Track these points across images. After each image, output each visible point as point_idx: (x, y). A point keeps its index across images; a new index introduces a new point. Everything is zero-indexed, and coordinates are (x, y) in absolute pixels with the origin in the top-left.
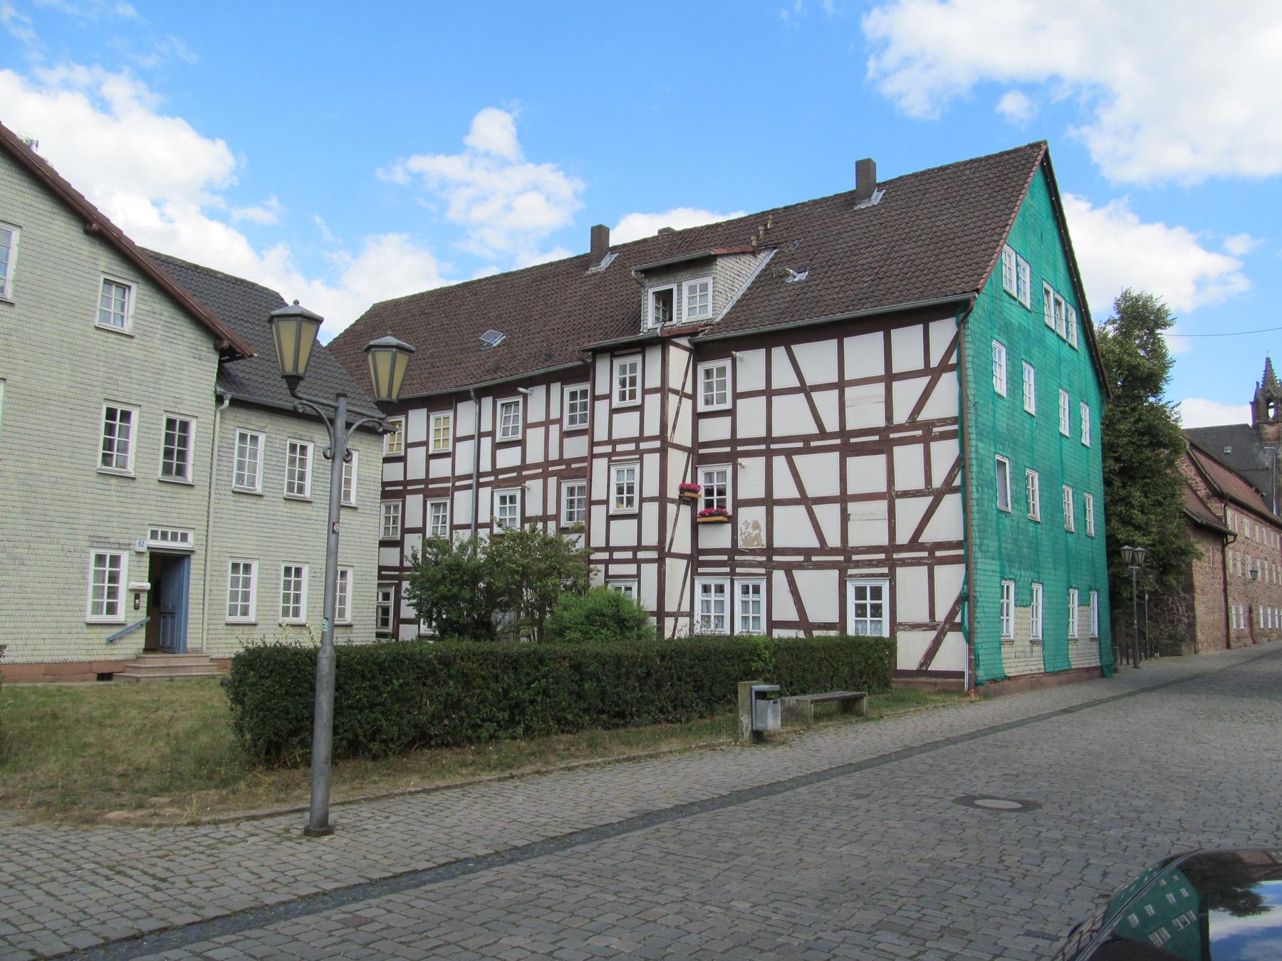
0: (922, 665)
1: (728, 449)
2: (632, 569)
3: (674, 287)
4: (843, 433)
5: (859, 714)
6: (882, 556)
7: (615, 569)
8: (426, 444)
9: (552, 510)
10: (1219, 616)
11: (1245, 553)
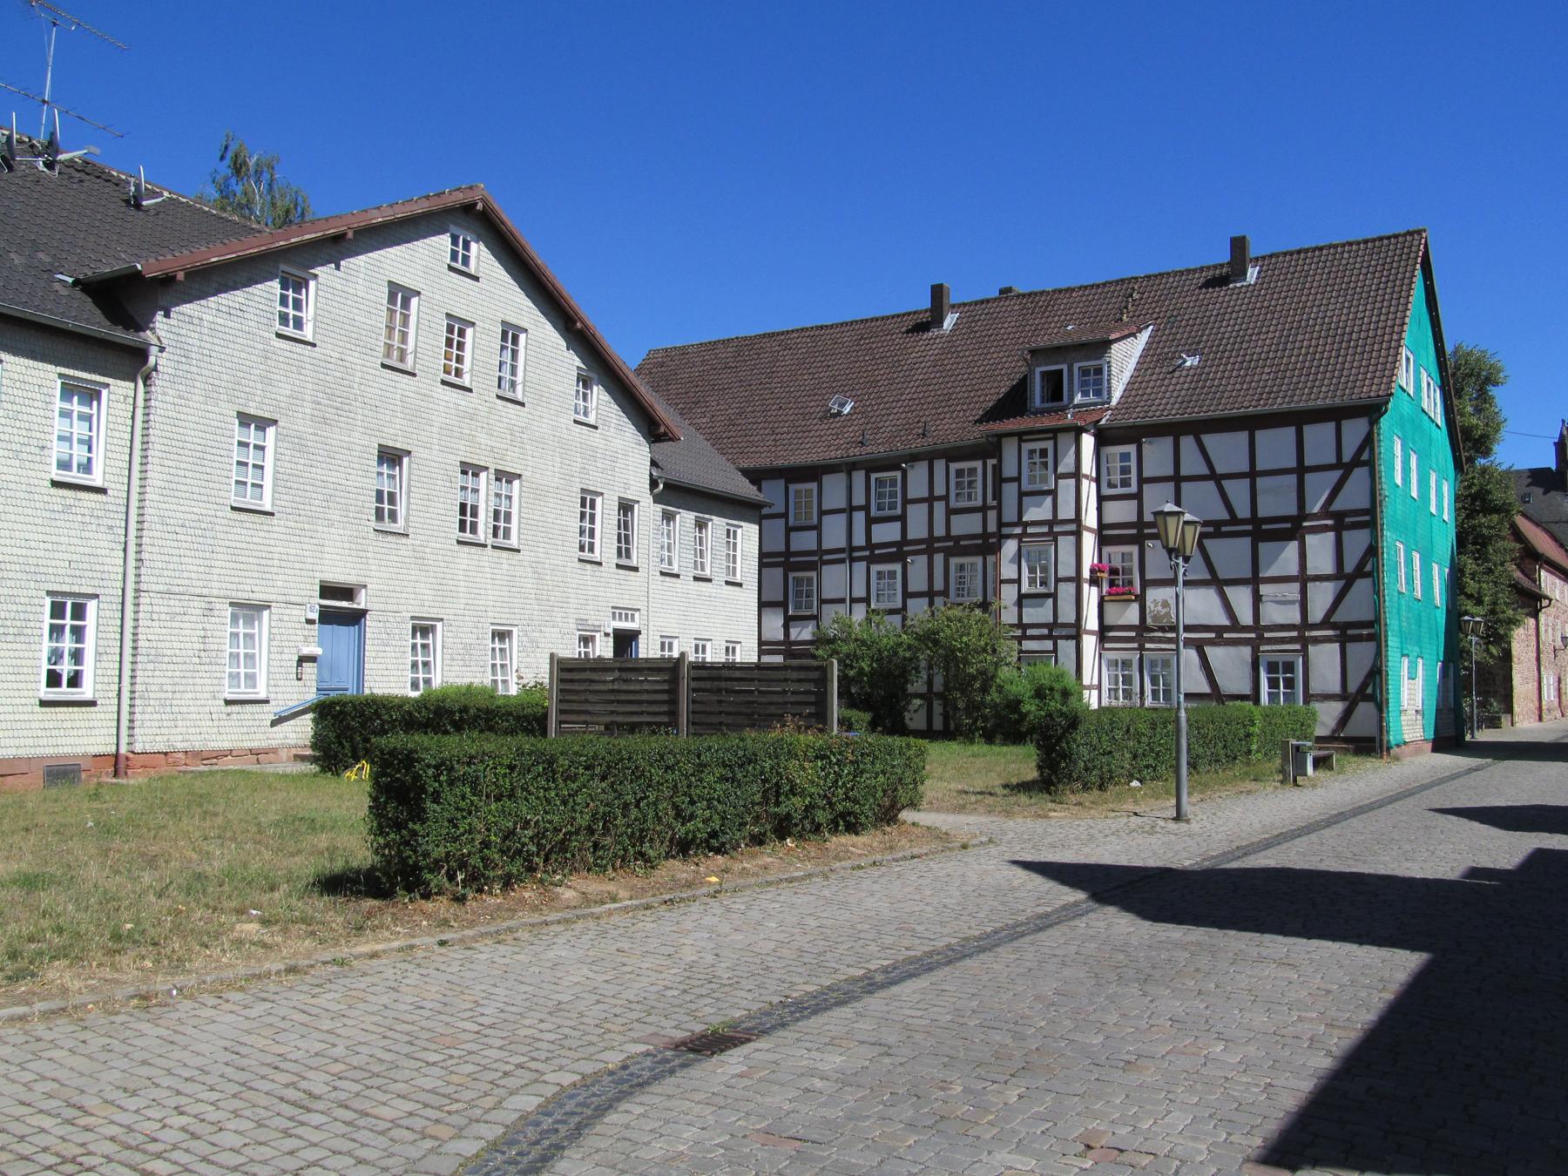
0: (1334, 731)
1: (1134, 531)
2: (1049, 645)
3: (1064, 367)
4: (1254, 519)
5: (1331, 768)
6: (1295, 634)
7: (1028, 645)
8: (785, 515)
9: (939, 585)
10: (1533, 686)
11: (1556, 617)
